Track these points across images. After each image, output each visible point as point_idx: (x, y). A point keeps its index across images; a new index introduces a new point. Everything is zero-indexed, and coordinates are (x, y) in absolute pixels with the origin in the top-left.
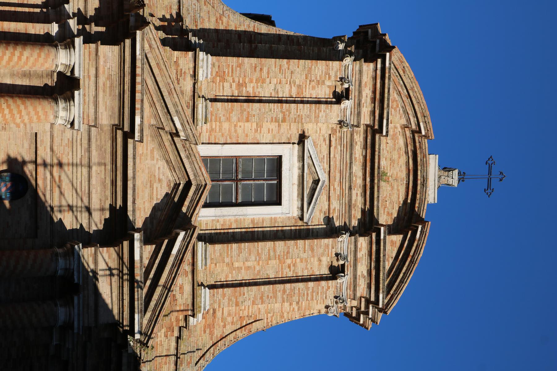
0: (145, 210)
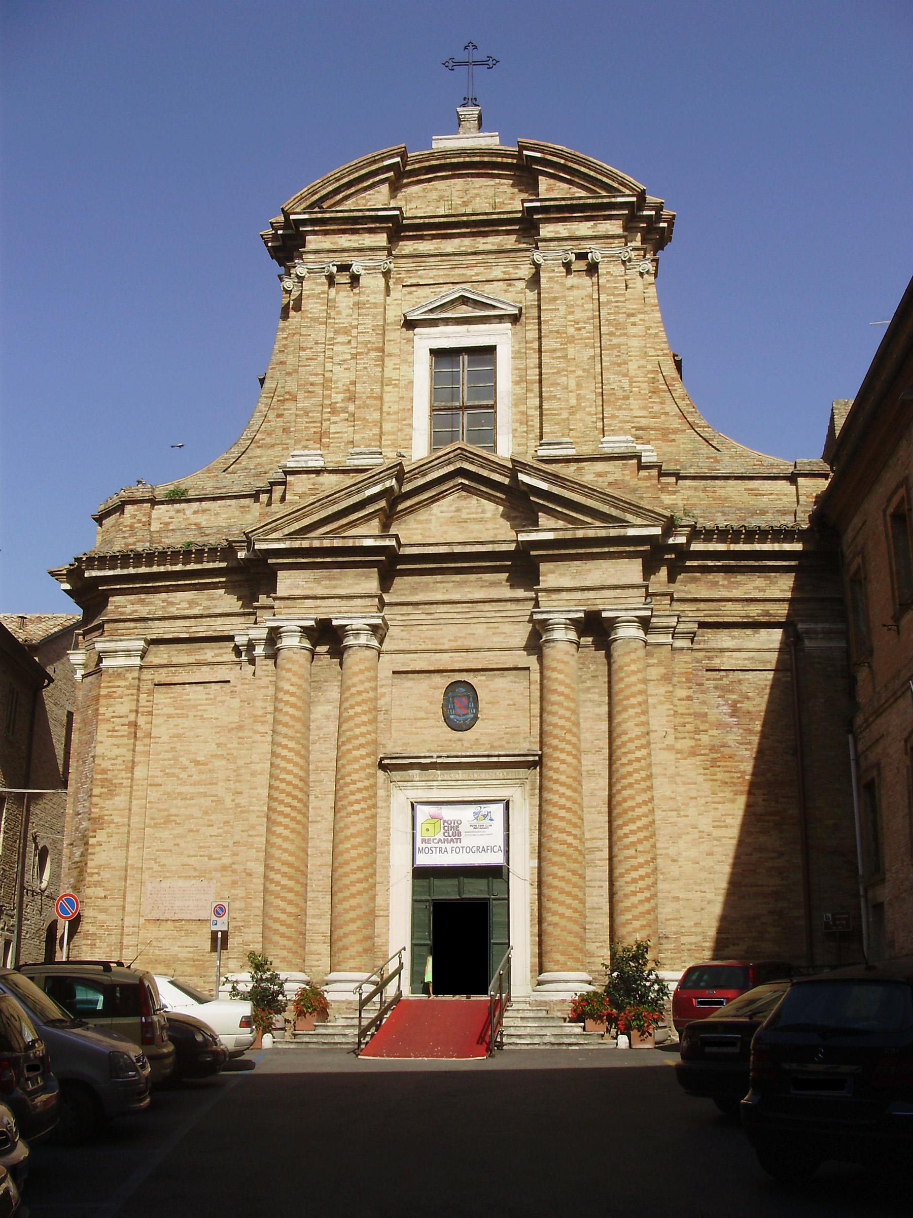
0: (497, 528)
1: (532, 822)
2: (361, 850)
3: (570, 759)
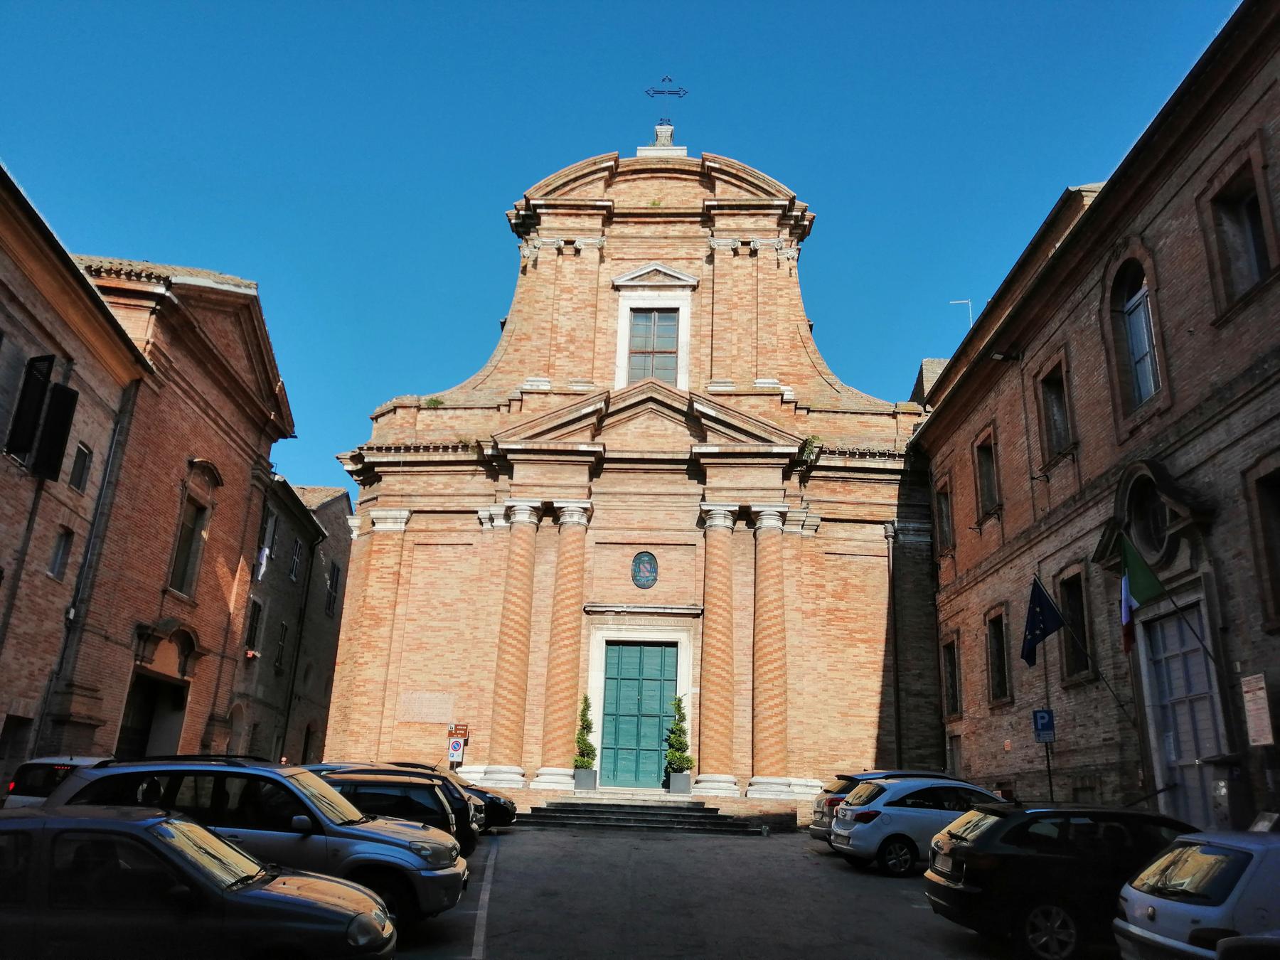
1: (694, 659)
2: (568, 675)
3: (725, 614)
